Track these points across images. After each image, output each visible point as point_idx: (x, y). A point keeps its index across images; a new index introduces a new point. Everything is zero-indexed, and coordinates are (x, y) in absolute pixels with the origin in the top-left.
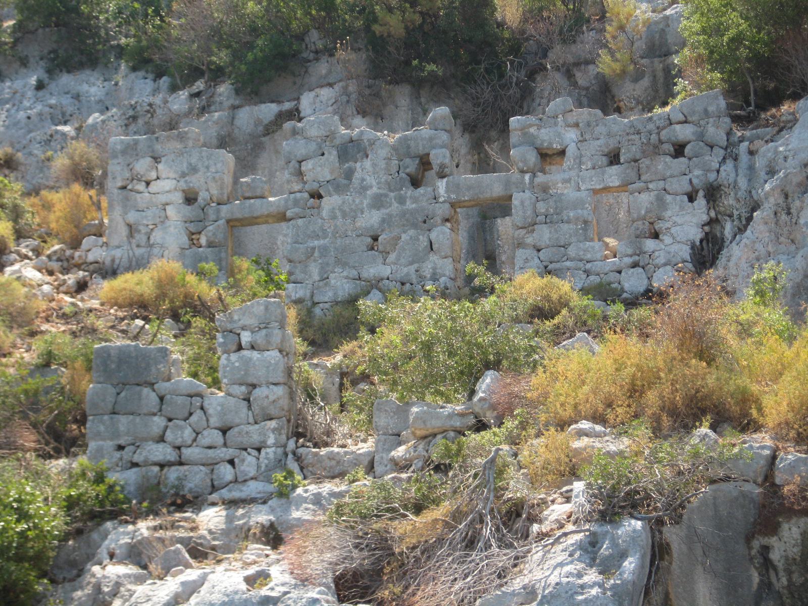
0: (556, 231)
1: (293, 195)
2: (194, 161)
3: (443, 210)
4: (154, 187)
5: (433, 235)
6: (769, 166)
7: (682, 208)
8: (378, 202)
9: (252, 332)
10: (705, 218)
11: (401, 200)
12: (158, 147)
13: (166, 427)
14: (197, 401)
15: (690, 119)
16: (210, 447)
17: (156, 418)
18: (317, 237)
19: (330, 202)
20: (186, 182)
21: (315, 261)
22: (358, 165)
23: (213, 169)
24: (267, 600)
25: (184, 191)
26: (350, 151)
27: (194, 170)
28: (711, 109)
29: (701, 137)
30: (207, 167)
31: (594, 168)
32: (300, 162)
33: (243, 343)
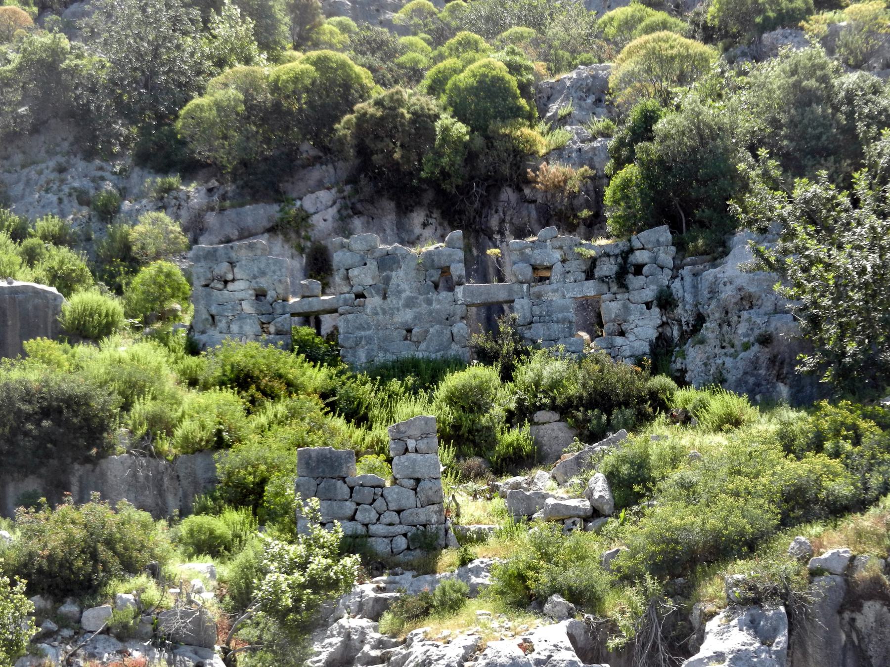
0: (548, 329)
1: (342, 296)
2: (262, 266)
3: (460, 310)
4: (231, 286)
5: (455, 330)
6: (710, 287)
7: (642, 314)
8: (410, 303)
9: (416, 440)
10: (659, 322)
11: (429, 302)
12: (233, 255)
13: (357, 510)
14: (378, 491)
15: (646, 246)
16: (390, 525)
17: (348, 503)
18: (364, 329)
19: (373, 301)
20: (257, 282)
21: (362, 347)
22: (394, 273)
23: (278, 273)
24: (538, 662)
25: (255, 290)
26: (387, 262)
27: (263, 273)
28: (661, 239)
29: (655, 260)
30: (274, 272)
31: (575, 281)
32: (347, 270)
33: (410, 449)
